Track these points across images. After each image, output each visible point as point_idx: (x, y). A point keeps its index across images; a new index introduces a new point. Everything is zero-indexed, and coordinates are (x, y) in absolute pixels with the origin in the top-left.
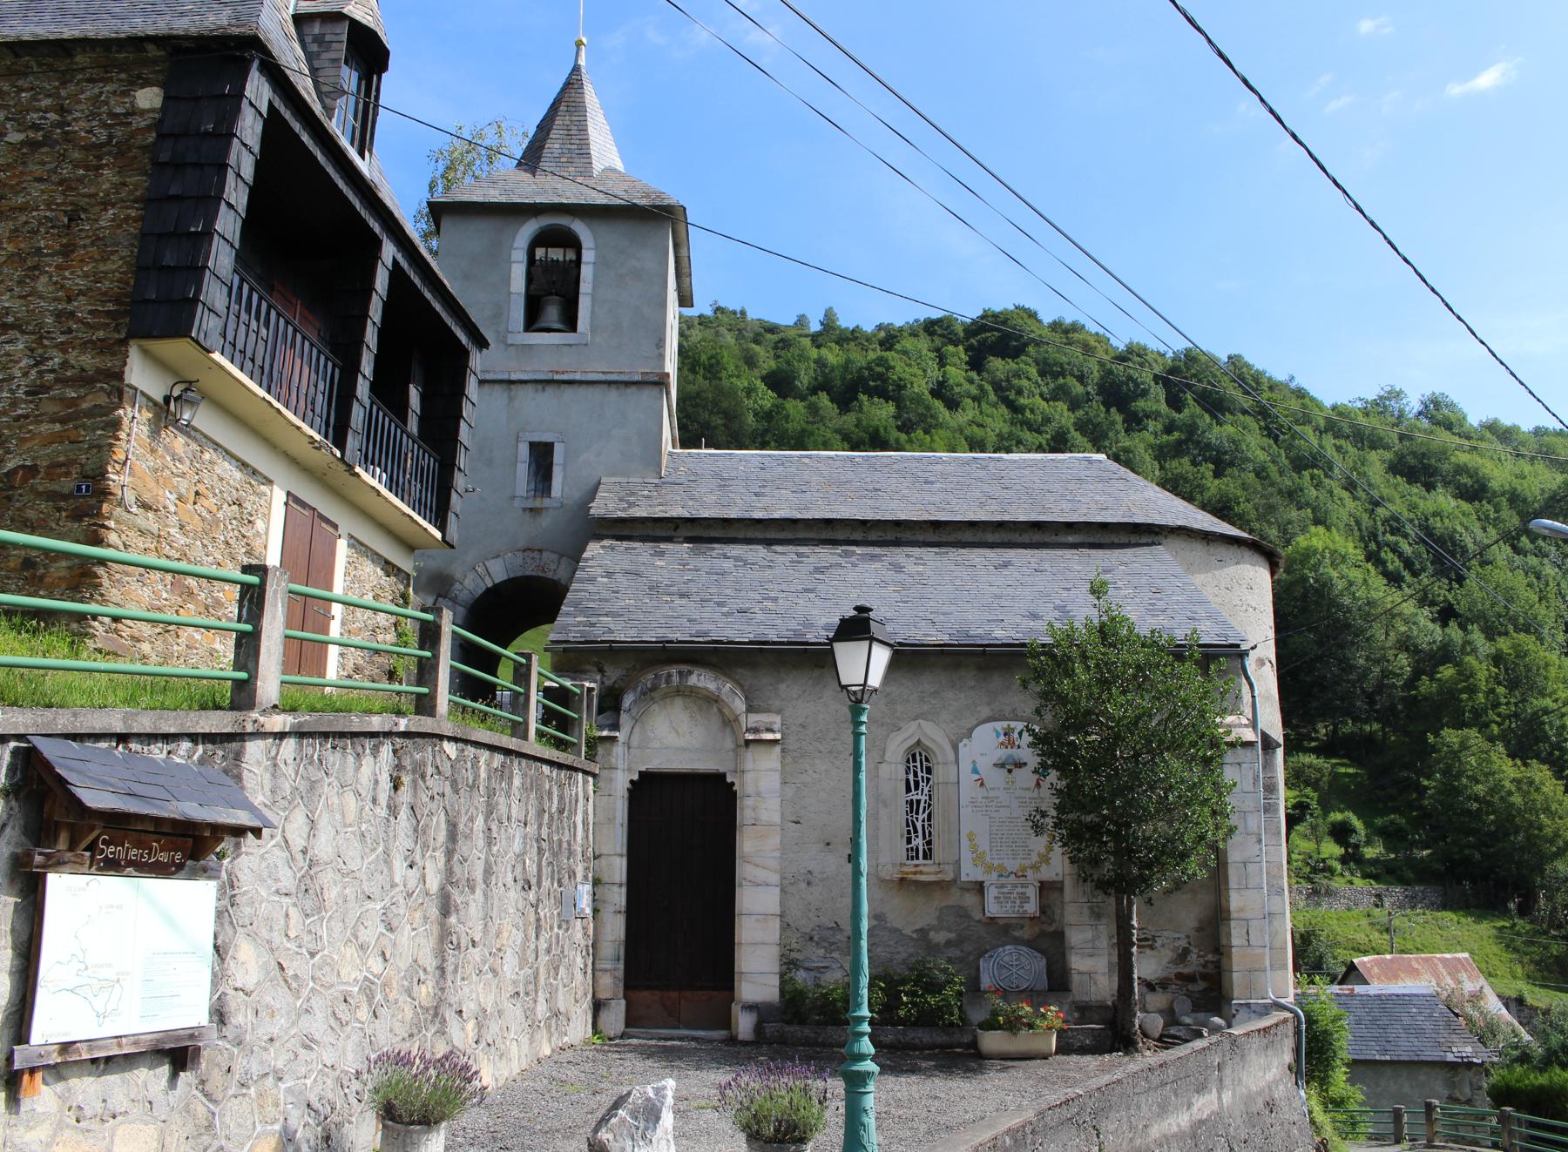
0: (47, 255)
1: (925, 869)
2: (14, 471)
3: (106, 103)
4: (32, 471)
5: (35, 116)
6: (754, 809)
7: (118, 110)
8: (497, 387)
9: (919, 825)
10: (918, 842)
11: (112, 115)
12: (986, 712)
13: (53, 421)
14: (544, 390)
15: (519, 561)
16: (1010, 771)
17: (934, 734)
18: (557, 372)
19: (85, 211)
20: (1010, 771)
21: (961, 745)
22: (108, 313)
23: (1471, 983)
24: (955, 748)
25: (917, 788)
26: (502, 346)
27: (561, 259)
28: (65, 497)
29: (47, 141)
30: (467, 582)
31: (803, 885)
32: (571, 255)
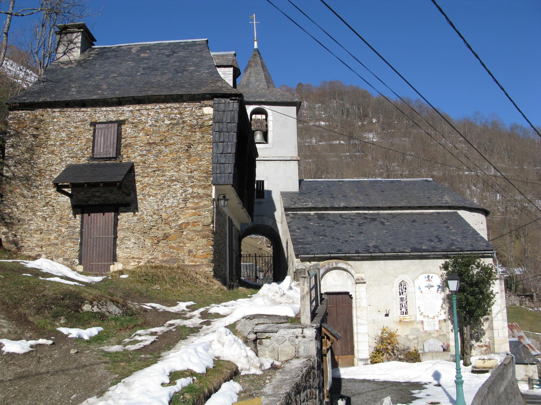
0: (183, 159)
1: (406, 318)
2: (182, 224)
3: (195, 112)
4: (188, 223)
5: (173, 115)
6: (359, 303)
7: (199, 114)
9: (404, 305)
10: (404, 310)
11: (197, 116)
12: (422, 271)
13: (192, 209)
16: (429, 288)
17: (407, 278)
19: (192, 145)
20: (429, 288)
21: (415, 281)
22: (204, 177)
23: (129, 198)
24: (414, 282)
25: (402, 294)
27: (261, 118)
28: (198, 232)
29: (177, 124)
31: (372, 324)
32: (264, 117)
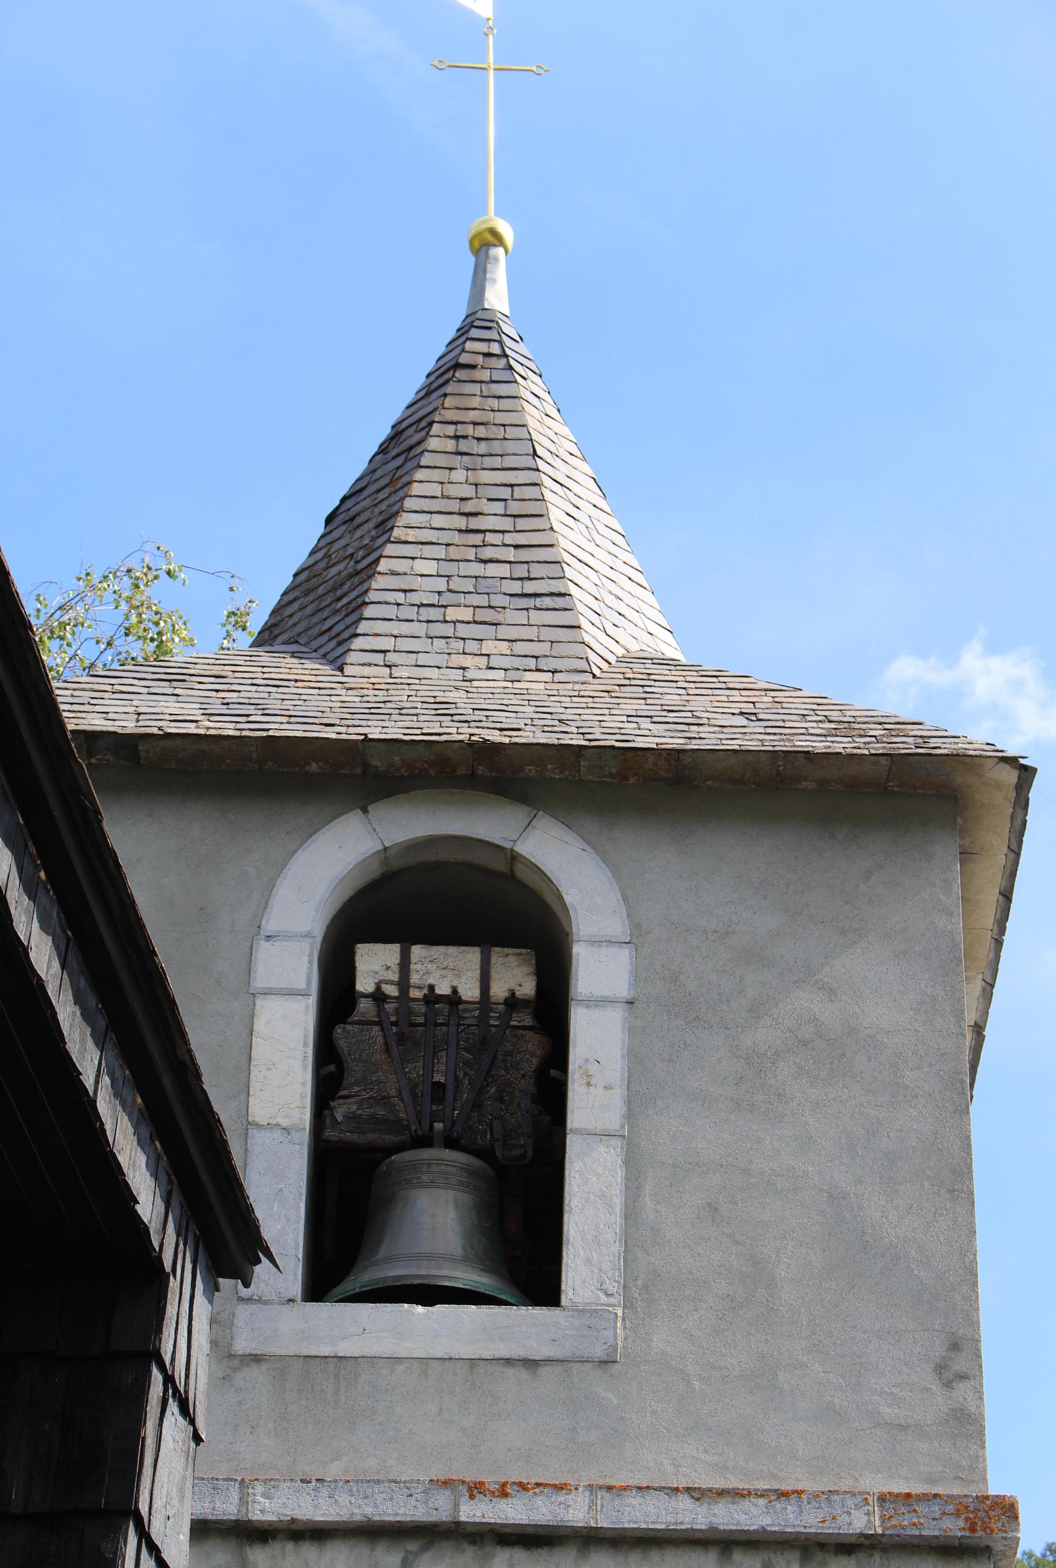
18: (476, 1489)
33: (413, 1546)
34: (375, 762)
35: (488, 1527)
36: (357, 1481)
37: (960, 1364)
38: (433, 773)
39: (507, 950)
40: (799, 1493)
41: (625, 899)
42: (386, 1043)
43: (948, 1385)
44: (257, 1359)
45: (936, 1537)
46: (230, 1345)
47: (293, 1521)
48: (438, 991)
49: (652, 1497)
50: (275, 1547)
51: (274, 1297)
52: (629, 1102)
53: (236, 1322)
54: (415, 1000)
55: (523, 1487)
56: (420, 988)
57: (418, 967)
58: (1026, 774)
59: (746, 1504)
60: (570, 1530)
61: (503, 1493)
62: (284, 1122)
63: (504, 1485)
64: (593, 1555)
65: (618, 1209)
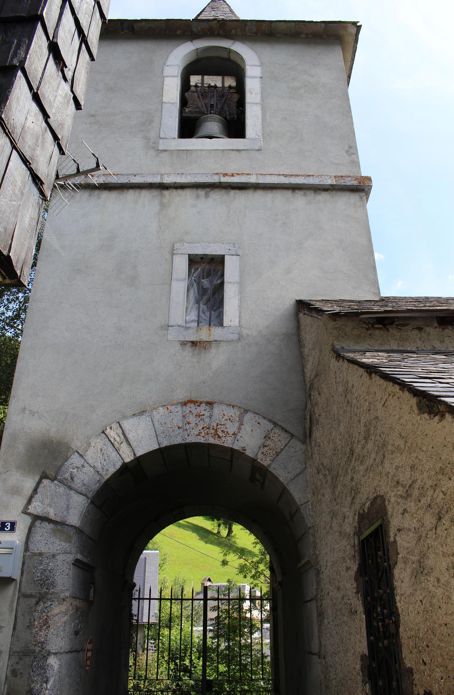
8: (145, 193)
14: (207, 196)
15: (177, 420)
18: (225, 175)
26: (152, 152)
27: (219, 85)
30: (90, 455)
32: (230, 82)
33: (208, 190)
34: (194, 30)
35: (229, 184)
36: (193, 174)
37: (352, 151)
38: (209, 33)
39: (228, 77)
40: (313, 175)
41: (259, 58)
42: (198, 96)
43: (350, 155)
44: (165, 151)
45: (350, 185)
46: (158, 148)
47: (175, 183)
48: (211, 85)
49: (273, 176)
50: (171, 191)
51: (169, 138)
52: (262, 97)
53: (159, 143)
54: (205, 87)
55: (238, 174)
56: (206, 84)
57: (206, 80)
58: (360, 27)
59: (299, 177)
60: (251, 184)
61: (233, 175)
62: (172, 102)
63: (233, 174)
64: (257, 191)
65: (260, 119)
